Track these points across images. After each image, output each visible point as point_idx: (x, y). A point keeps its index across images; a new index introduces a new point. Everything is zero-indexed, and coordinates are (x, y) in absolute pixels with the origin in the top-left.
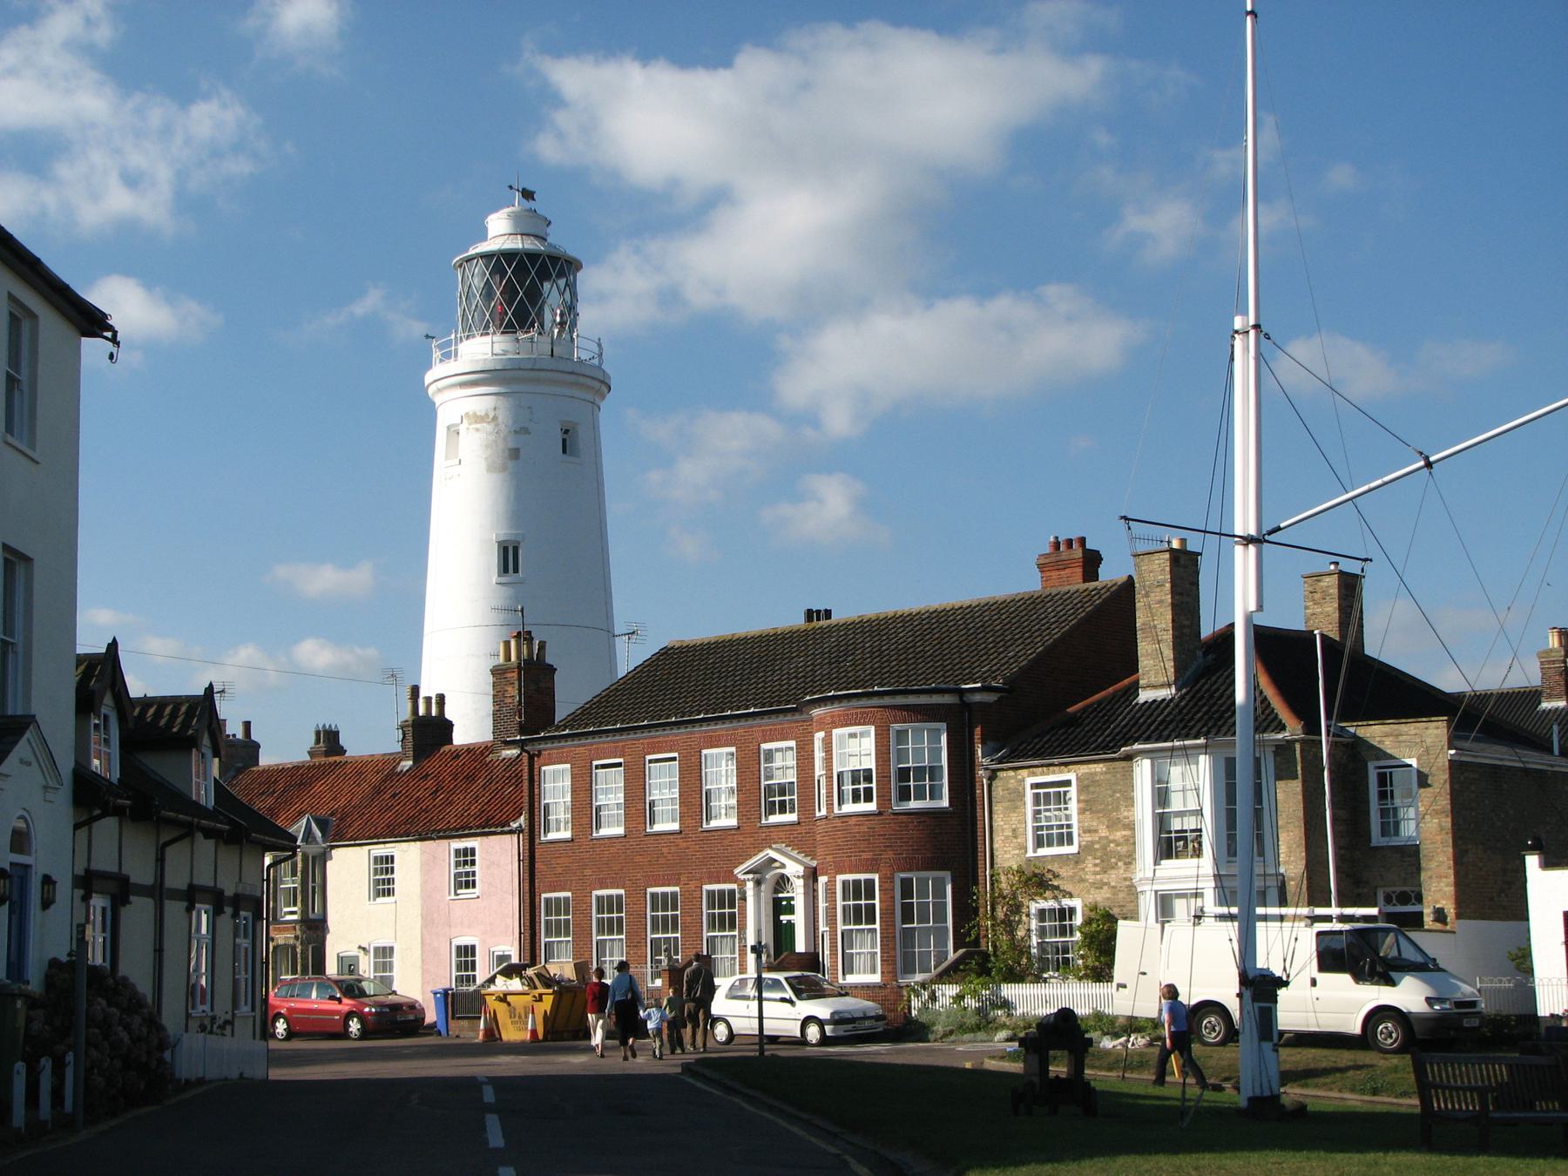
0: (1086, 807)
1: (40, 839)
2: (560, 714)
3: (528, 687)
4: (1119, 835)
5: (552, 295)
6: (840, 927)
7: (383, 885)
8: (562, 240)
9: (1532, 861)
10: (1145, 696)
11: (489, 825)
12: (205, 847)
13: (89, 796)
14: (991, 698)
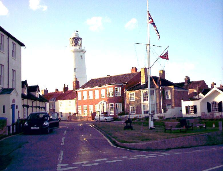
1: (16, 101)
2: (80, 87)
3: (77, 84)
4: (139, 99)
5: (80, 42)
6: (110, 109)
8: (80, 36)
9: (182, 101)
10: (142, 84)
12: (38, 102)
13: (23, 97)
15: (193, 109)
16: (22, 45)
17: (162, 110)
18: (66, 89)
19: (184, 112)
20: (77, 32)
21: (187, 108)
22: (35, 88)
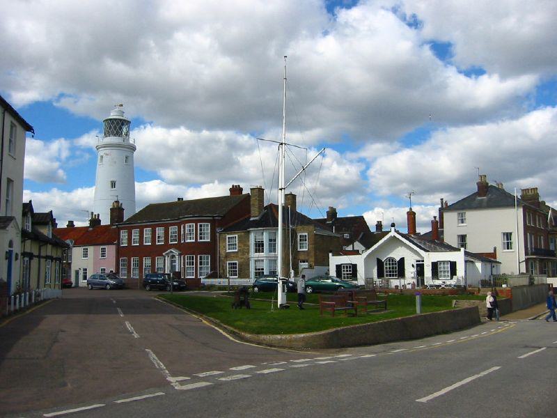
0: (239, 242)
3: (117, 211)
7: (86, 255)
9: (330, 254)
11: (109, 243)
12: (49, 247)
13: (25, 235)
14: (220, 218)
15: (350, 271)
16: (28, 128)
17: (292, 271)
18: (95, 221)
19: (333, 273)
20: (121, 108)
21: (339, 267)
22: (48, 219)
